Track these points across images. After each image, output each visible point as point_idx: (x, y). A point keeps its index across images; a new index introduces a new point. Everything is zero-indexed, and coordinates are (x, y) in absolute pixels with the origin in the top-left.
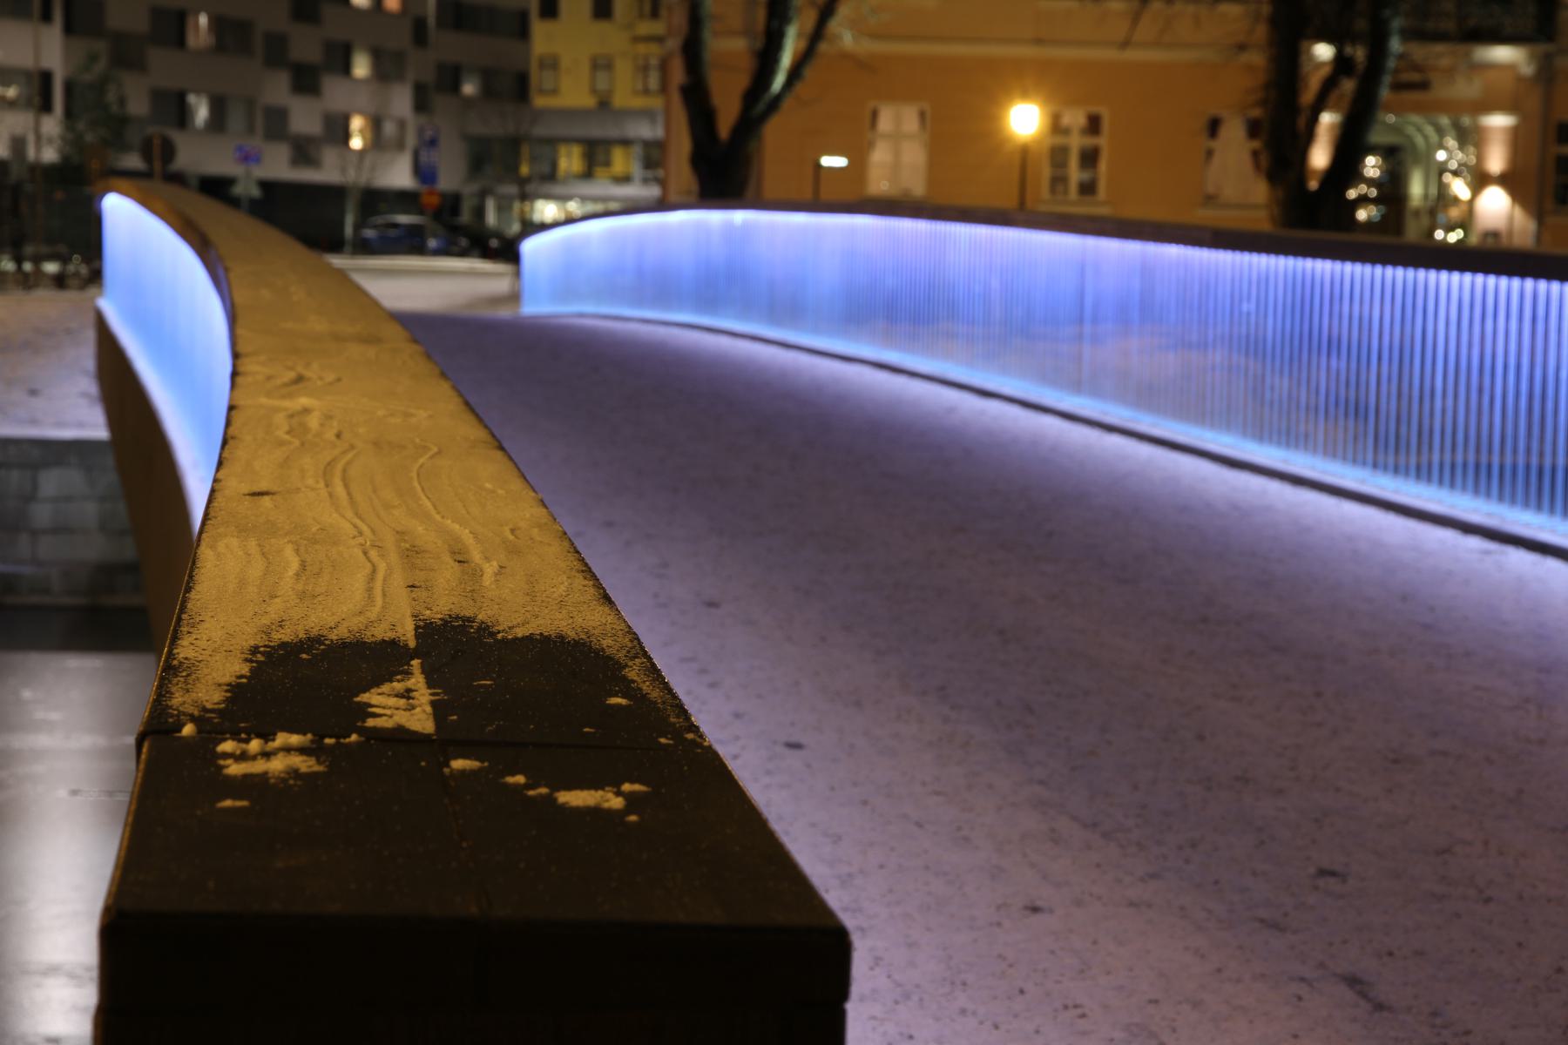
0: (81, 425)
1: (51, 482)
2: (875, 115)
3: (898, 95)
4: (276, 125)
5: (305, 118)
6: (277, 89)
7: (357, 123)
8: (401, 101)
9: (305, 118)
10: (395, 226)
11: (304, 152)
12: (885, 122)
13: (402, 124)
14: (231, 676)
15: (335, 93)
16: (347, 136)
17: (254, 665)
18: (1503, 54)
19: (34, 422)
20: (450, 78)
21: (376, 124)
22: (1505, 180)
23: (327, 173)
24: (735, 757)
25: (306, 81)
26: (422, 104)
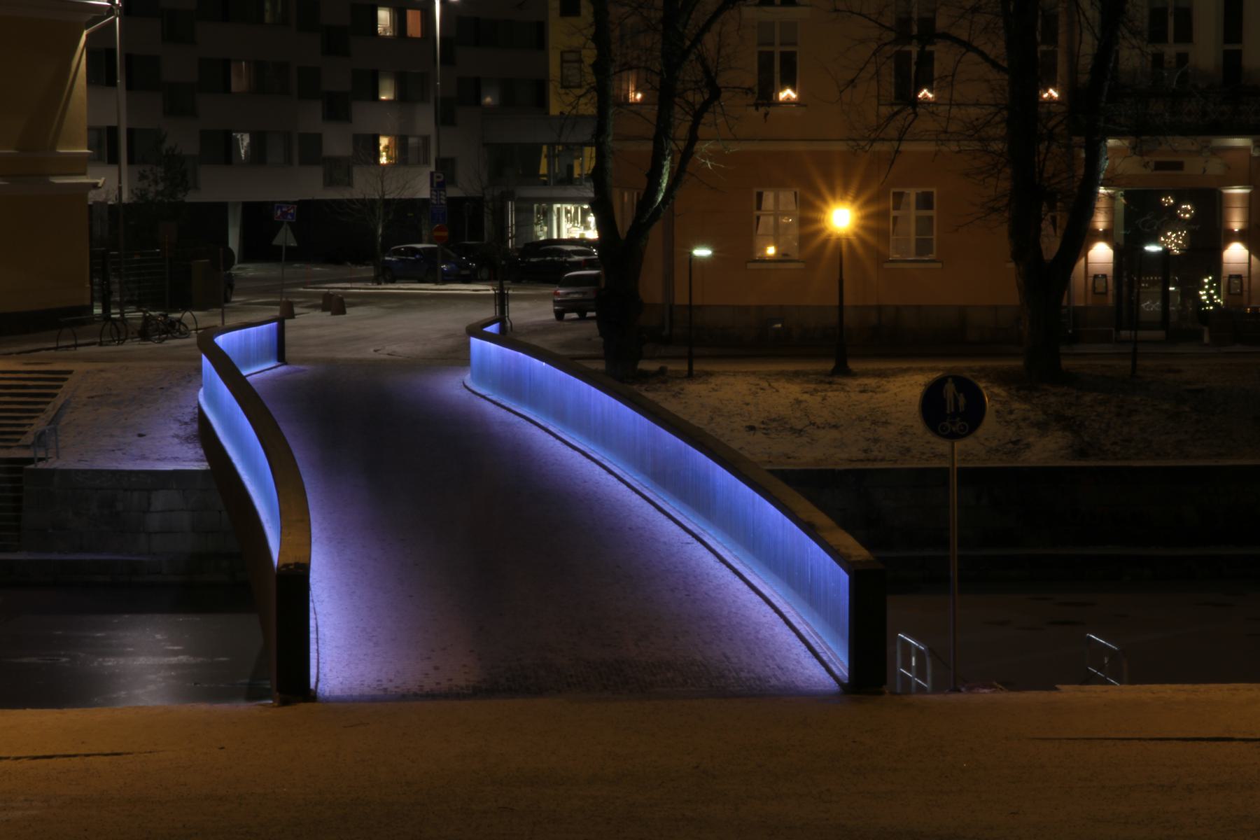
0: (176, 459)
1: (160, 500)
2: (760, 196)
3: (778, 185)
4: (311, 151)
5: (336, 143)
6: (311, 119)
7: (384, 141)
8: (425, 121)
9: (336, 143)
10: (415, 251)
11: (338, 172)
12: (769, 200)
13: (426, 139)
14: (181, 429)
15: (363, 119)
16: (377, 155)
17: (688, 43)
18: (1239, 142)
19: (143, 457)
20: (470, 91)
21: (401, 144)
22: (1243, 237)
23: (362, 188)
24: (800, 646)
25: (337, 110)
26: (445, 118)
